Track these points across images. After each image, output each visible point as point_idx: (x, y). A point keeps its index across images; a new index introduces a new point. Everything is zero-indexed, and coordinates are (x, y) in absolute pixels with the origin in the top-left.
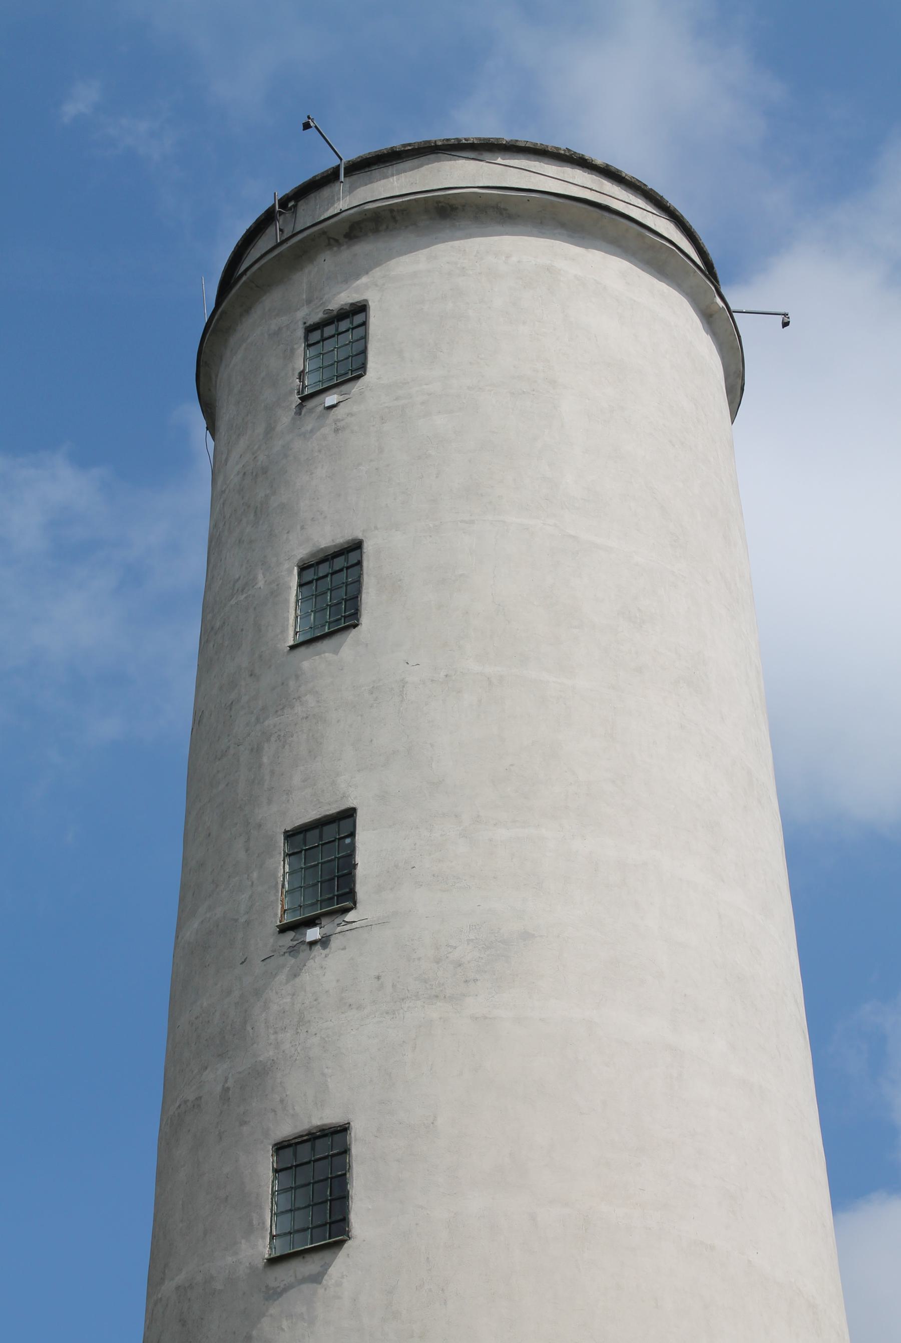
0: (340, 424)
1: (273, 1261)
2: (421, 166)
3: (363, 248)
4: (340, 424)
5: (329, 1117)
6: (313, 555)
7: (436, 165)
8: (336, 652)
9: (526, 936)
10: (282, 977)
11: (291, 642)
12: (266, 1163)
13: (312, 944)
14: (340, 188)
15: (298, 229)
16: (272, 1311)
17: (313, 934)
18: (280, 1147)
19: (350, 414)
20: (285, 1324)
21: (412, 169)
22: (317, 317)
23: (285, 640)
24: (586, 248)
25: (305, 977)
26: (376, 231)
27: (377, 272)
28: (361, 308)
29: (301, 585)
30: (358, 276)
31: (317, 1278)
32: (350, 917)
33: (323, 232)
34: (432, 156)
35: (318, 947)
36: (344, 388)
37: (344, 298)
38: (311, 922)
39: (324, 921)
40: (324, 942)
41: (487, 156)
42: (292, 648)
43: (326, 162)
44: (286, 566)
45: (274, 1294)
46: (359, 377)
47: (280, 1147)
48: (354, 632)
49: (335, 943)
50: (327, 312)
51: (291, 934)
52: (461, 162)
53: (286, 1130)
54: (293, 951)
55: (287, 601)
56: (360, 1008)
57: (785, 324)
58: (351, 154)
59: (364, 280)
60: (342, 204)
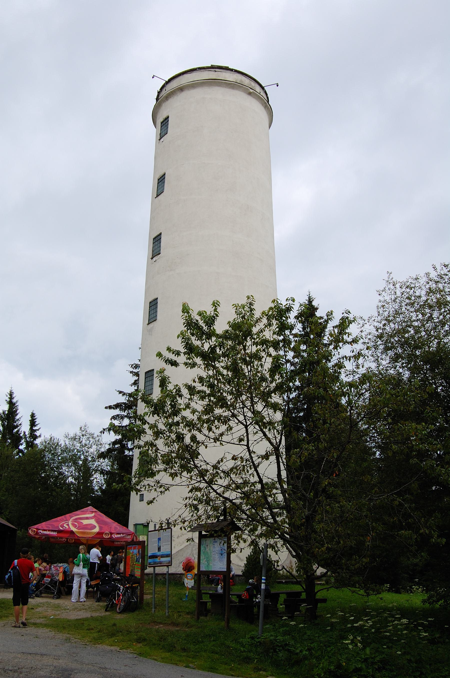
22: (162, 120)
37: (165, 116)
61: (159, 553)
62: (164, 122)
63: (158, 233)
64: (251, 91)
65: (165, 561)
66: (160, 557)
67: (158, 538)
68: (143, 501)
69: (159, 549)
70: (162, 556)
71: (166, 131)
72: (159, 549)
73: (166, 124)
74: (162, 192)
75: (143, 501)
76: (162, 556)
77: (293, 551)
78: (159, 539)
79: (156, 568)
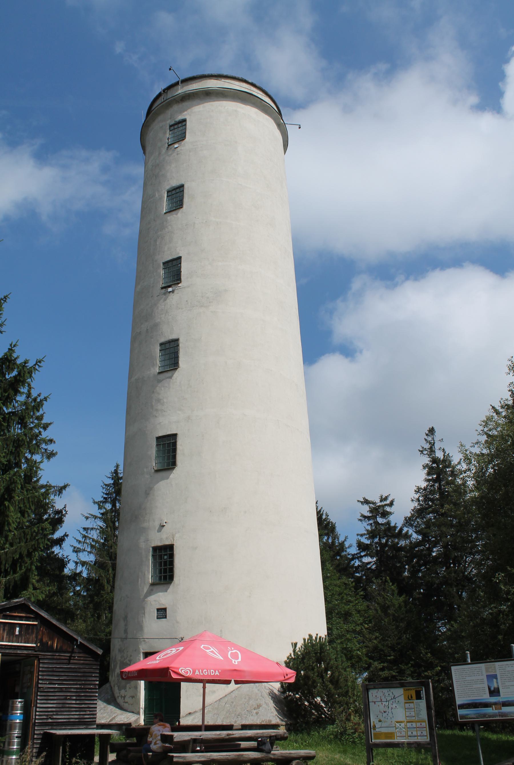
0: (179, 152)
1: (159, 373)
2: (201, 81)
3: (186, 104)
5: (174, 337)
6: (171, 188)
7: (206, 81)
8: (177, 214)
11: (165, 212)
17: (170, 289)
20: (162, 389)
22: (173, 123)
25: (168, 301)
27: (189, 111)
28: (185, 121)
30: (184, 112)
31: (171, 377)
32: (179, 285)
33: (175, 99)
35: (171, 293)
36: (180, 143)
37: (180, 118)
38: (170, 286)
39: (173, 286)
40: (173, 292)
45: (160, 381)
46: (184, 140)
47: (161, 344)
49: (176, 292)
50: (175, 121)
51: (164, 290)
52: (213, 80)
53: (163, 340)
55: (164, 201)
56: (182, 309)
57: (300, 128)
58: (182, 78)
59: (185, 113)
60: (180, 91)
61: (493, 699)
66: (499, 706)
67: (487, 676)
68: (166, 618)
69: (494, 692)
72: (494, 692)
75: (166, 618)
78: (492, 677)
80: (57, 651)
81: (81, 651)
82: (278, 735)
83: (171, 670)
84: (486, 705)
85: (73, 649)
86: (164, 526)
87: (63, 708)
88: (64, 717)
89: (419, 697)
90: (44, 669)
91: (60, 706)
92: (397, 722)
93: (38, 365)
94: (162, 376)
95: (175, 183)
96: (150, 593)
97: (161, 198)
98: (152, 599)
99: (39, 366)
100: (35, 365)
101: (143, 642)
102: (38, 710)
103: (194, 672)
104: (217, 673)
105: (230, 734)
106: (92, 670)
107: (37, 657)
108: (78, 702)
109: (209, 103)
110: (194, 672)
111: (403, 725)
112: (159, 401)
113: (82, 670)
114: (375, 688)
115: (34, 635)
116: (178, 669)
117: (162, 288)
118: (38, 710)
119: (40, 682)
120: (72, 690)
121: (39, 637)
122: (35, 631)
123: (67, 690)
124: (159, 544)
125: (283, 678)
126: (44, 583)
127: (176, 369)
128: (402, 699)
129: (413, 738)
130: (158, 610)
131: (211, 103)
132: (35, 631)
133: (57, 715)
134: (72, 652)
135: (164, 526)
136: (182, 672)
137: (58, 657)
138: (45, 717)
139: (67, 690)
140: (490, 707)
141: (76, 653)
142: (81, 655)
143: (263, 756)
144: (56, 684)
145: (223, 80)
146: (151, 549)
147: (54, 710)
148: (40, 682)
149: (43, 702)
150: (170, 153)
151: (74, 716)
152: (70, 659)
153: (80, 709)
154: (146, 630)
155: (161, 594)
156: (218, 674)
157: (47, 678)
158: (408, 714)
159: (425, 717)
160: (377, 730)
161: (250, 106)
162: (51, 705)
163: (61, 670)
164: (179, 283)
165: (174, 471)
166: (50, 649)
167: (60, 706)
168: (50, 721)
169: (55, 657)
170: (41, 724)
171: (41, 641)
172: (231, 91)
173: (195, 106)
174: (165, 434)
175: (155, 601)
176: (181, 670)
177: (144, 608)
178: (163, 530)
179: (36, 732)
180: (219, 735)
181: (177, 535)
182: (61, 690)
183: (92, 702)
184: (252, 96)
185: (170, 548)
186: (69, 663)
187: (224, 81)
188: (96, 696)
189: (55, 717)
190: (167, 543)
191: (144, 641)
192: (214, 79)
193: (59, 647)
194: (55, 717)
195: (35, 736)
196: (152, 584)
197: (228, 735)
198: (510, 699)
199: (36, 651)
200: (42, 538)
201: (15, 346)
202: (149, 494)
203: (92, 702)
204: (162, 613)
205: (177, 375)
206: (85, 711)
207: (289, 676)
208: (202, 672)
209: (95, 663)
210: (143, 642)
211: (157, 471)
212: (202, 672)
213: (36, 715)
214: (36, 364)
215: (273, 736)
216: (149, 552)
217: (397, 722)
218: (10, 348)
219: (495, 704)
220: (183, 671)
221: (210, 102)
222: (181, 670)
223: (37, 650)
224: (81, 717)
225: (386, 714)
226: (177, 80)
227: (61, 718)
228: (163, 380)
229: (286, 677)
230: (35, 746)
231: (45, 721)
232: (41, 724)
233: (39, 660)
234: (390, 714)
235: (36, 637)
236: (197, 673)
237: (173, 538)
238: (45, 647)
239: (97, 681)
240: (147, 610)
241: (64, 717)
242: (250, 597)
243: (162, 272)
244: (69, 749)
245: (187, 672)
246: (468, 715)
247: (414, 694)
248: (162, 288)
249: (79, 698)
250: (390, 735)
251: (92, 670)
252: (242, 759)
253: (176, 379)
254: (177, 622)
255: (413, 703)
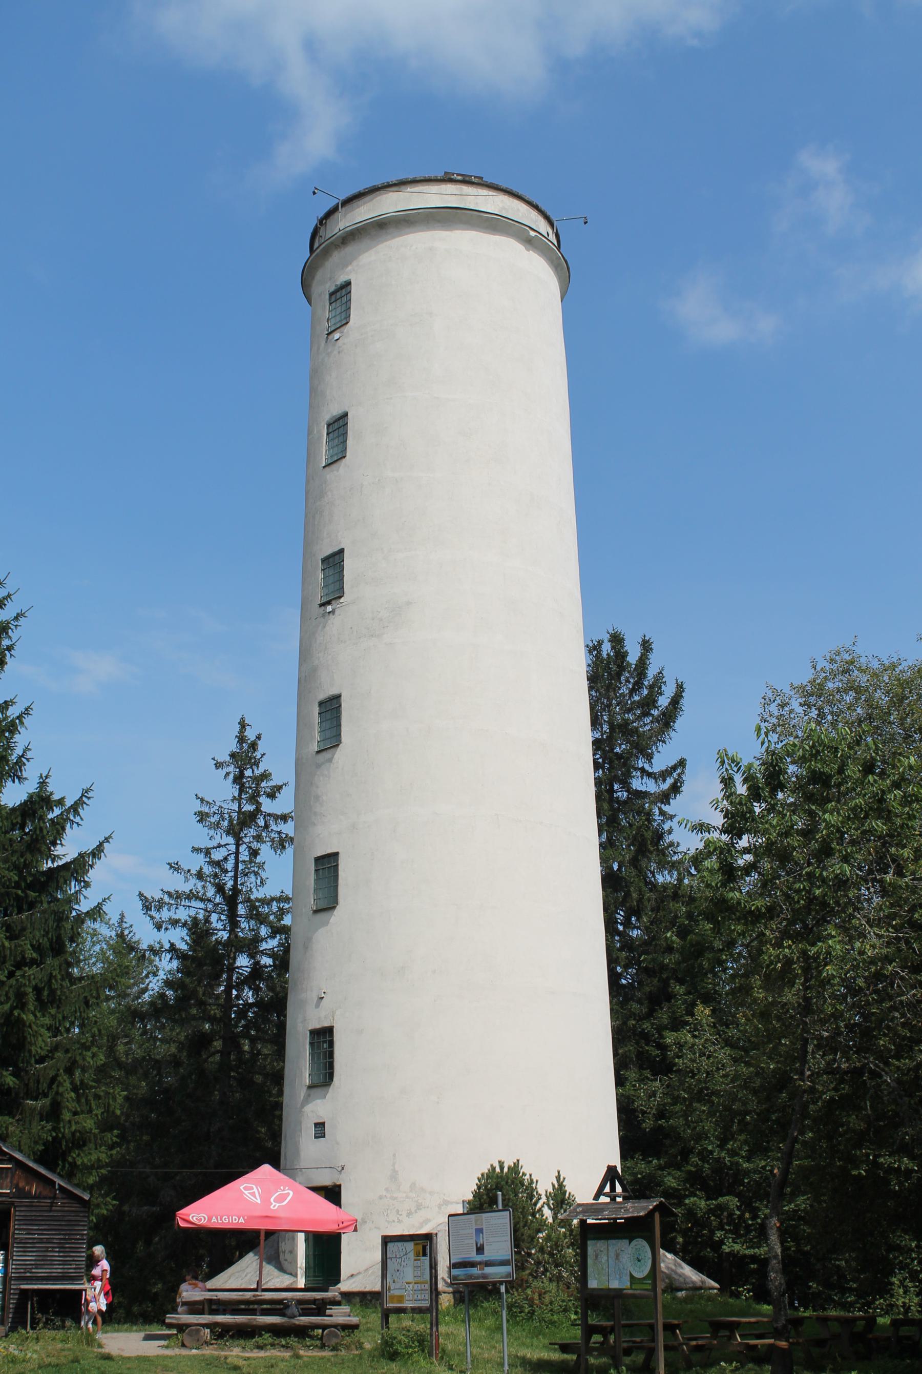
0: (341, 349)
1: (318, 752)
2: (373, 199)
3: (349, 249)
4: (341, 349)
5: (334, 691)
6: (331, 419)
7: (379, 198)
8: (338, 471)
9: (409, 603)
10: (320, 628)
11: (324, 465)
12: (316, 710)
13: (329, 613)
14: (338, 215)
15: (327, 238)
16: (318, 773)
17: (329, 608)
18: (321, 704)
19: (344, 344)
20: (321, 778)
21: (369, 201)
22: (333, 289)
23: (322, 463)
24: (451, 230)
25: (327, 628)
26: (354, 239)
27: (355, 263)
28: (348, 284)
29: (328, 434)
30: (347, 266)
31: (330, 760)
32: (342, 600)
33: (332, 243)
34: (378, 193)
35: (331, 614)
36: (342, 329)
37: (342, 279)
38: (329, 603)
39: (333, 602)
40: (333, 612)
41: (403, 188)
42: (324, 467)
43: (332, 203)
44: (322, 424)
45: (318, 766)
46: (347, 323)
47: (321, 704)
48: (344, 460)
49: (337, 612)
50: (336, 285)
51: (323, 607)
52: (391, 194)
53: (322, 696)
54: (323, 615)
55: (322, 443)
56: (345, 642)
57: (586, 223)
58: (343, 197)
59: (350, 268)
60: (341, 225)
61: (479, 1258)
62: (338, 295)
63: (336, 549)
64: (532, 234)
65: (496, 1274)
66: (482, 1266)
67: (476, 1229)
68: (324, 1137)
69: (480, 1250)
70: (488, 1264)
71: (343, 315)
72: (480, 1250)
73: (344, 299)
74: (341, 458)
75: (324, 1137)
76: (488, 1264)
77: (268, 1306)
78: (479, 1231)
79: (254, 1286)
80: (35, 1197)
81: (64, 1196)
82: (326, 1299)
83: (180, 1218)
84: (472, 1265)
85: (56, 1194)
86: (323, 998)
87: (43, 1261)
88: (44, 1271)
89: (424, 1254)
90: (20, 1218)
91: (41, 1258)
92: (407, 1283)
93: (86, 796)
94: (322, 757)
95: (335, 410)
96: (307, 1100)
97: (320, 437)
98: (309, 1108)
99: (89, 798)
100: (81, 797)
101: (300, 1173)
102: (14, 1263)
103: (210, 1219)
104: (242, 1220)
105: (258, 1295)
106: (78, 1218)
107: (12, 1204)
108: (61, 1254)
109: (385, 243)
110: (210, 1219)
111: (411, 1286)
112: (317, 798)
113: (66, 1218)
114: (594, 1239)
115: (9, 1180)
116: (189, 1215)
117: (322, 605)
118: (14, 1263)
119: (16, 1232)
120: (55, 1241)
121: (15, 1182)
122: (10, 1175)
123: (48, 1241)
124: (318, 1026)
125: (337, 1227)
126: (746, 976)
127: (337, 745)
128: (412, 1255)
129: (418, 1302)
130: (316, 1125)
131: (388, 243)
132: (10, 1175)
133: (36, 1268)
134: (55, 1197)
135: (323, 998)
136: (194, 1220)
137: (37, 1204)
138: (22, 1271)
139: (48, 1241)
140: (476, 1267)
141: (58, 1198)
142: (65, 1201)
143: (283, 1321)
144: (35, 1234)
145: (409, 190)
146: (308, 1033)
147: (33, 1263)
148: (16, 1232)
149: (19, 1254)
150: (329, 350)
151: (57, 1270)
152: (52, 1206)
153: (65, 1263)
154: (303, 1154)
155: (319, 1101)
156: (243, 1221)
157: (24, 1227)
158: (416, 1274)
159: (428, 1278)
160: (392, 1292)
161: (457, 229)
162: (30, 1257)
163: (40, 1218)
164: (340, 597)
165: (336, 912)
166: (28, 1195)
167: (41, 1258)
168: (28, 1274)
169: (34, 1204)
170: (18, 1279)
171: (17, 1186)
172: (419, 214)
173: (364, 252)
174: (324, 854)
175: (312, 1111)
176: (193, 1217)
177: (300, 1123)
178: (321, 1004)
179: (12, 1287)
180: (242, 1295)
181: (338, 1013)
182: (41, 1241)
183: (78, 1254)
184: (459, 211)
185: (327, 1032)
186: (51, 1211)
187: (413, 190)
188: (83, 1248)
189: (34, 1270)
190: (326, 1024)
191: (301, 1171)
192: (393, 191)
193: (38, 1192)
194: (34, 1270)
195: (12, 1292)
196: (310, 1087)
197: (254, 1296)
198: (492, 1258)
199: (11, 1198)
200: (79, 1049)
201: (46, 777)
202: (307, 948)
203: (78, 1254)
204: (320, 1129)
205: (340, 754)
206: (71, 1265)
207: (345, 1224)
208: (221, 1219)
209: (82, 1209)
210: (300, 1173)
211: (316, 912)
212: (221, 1219)
213: (12, 1269)
214: (83, 795)
215: (318, 1299)
216: (306, 1039)
217: (407, 1283)
218: (41, 780)
219: (480, 1263)
220: (194, 1218)
221: (386, 240)
222: (193, 1217)
223: (11, 1196)
224: (66, 1271)
225: (398, 1273)
226: (335, 202)
227: (42, 1272)
228: (323, 764)
229: (341, 1225)
230: (12, 1302)
231: (23, 1275)
232: (18, 1279)
233: (15, 1207)
234: (402, 1273)
235: (11, 1182)
236: (214, 1220)
237: (333, 1017)
238: (21, 1193)
239: (85, 1230)
240: (304, 1126)
241: (44, 1271)
242: (438, 1103)
243: (321, 576)
244: (37, 1303)
245: (201, 1219)
246: (458, 1275)
247: (420, 1248)
248: (322, 605)
249: (62, 1248)
250: (401, 1299)
251: (78, 1218)
252: (255, 1323)
253: (337, 762)
254: (338, 1144)
255: (419, 1260)
